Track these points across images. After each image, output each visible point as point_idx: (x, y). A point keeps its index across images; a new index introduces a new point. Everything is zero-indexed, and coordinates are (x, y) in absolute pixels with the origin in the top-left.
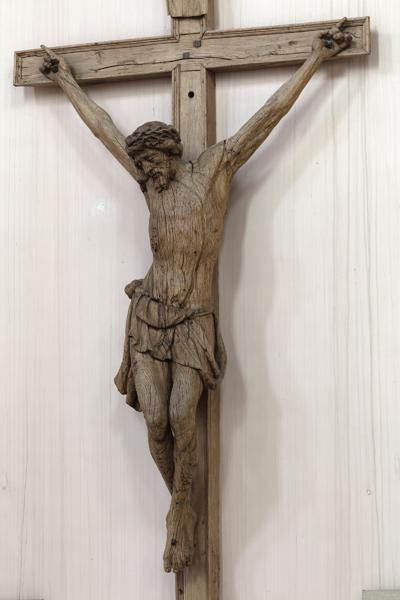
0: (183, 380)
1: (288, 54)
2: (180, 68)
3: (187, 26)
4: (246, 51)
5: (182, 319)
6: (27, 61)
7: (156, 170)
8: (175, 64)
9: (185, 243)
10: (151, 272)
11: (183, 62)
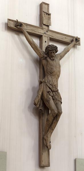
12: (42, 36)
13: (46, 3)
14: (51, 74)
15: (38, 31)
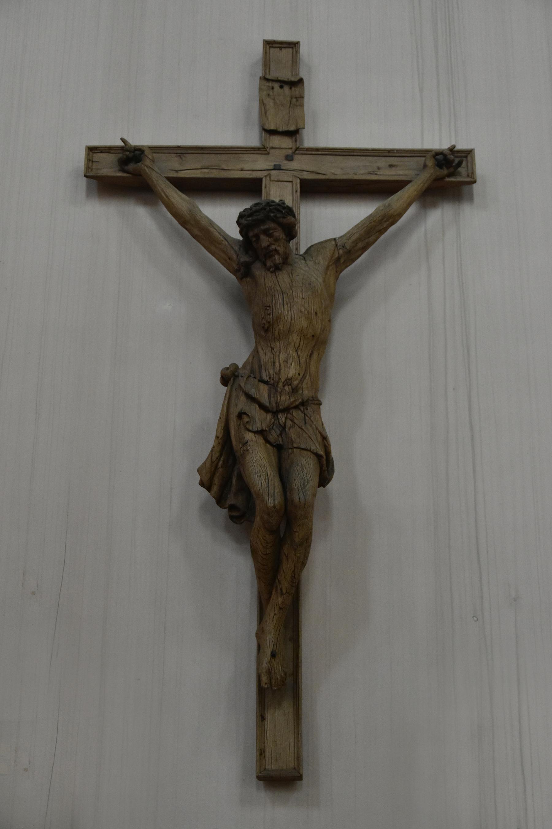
0: (267, 482)
1: (386, 174)
2: (270, 177)
3: (276, 141)
4: (342, 169)
5: (297, 403)
6: (97, 157)
7: (273, 247)
8: (265, 173)
9: (304, 323)
10: (255, 353)
11: (273, 173)
12: (259, 181)
13: (282, 43)
14: (267, 331)
15: (239, 167)
